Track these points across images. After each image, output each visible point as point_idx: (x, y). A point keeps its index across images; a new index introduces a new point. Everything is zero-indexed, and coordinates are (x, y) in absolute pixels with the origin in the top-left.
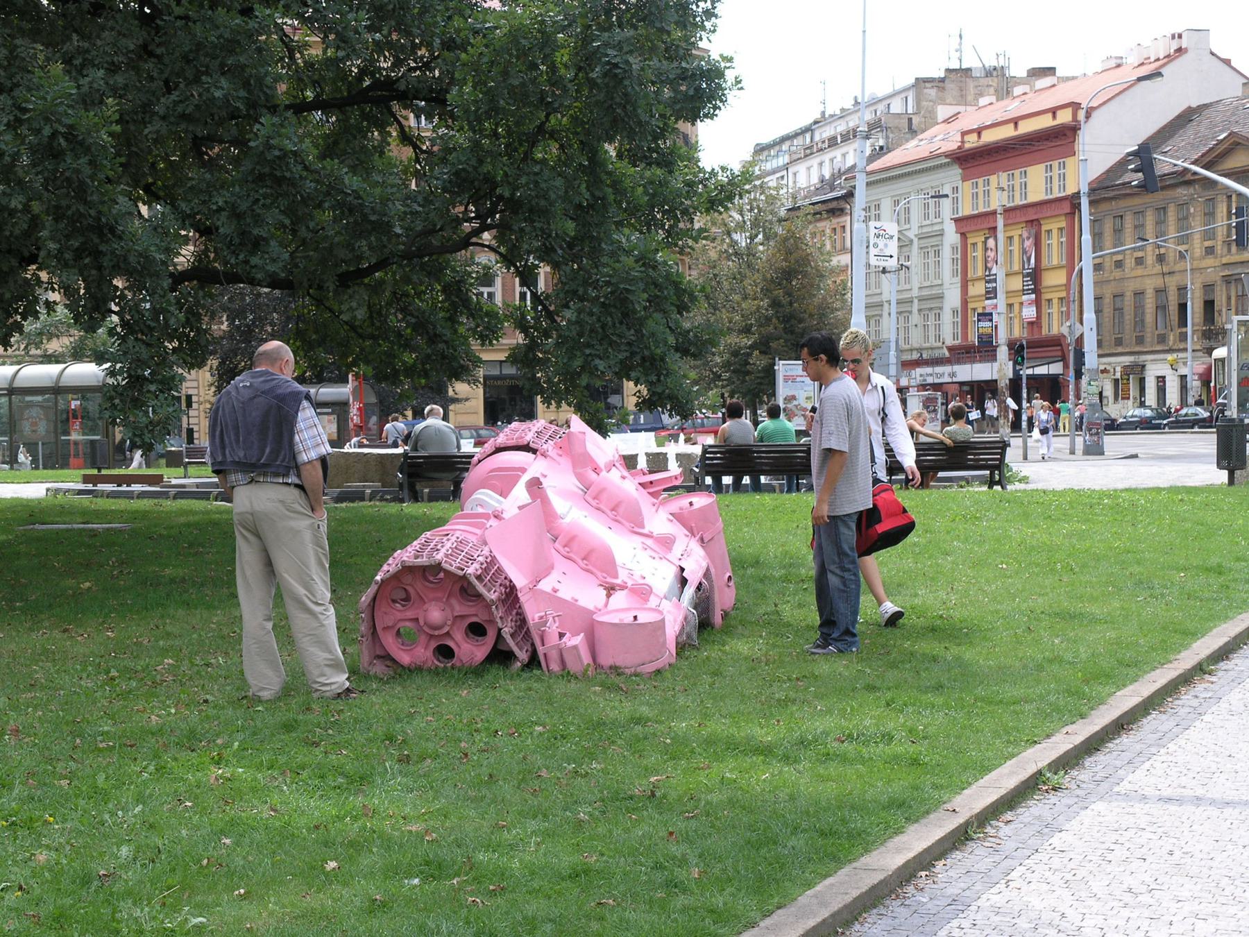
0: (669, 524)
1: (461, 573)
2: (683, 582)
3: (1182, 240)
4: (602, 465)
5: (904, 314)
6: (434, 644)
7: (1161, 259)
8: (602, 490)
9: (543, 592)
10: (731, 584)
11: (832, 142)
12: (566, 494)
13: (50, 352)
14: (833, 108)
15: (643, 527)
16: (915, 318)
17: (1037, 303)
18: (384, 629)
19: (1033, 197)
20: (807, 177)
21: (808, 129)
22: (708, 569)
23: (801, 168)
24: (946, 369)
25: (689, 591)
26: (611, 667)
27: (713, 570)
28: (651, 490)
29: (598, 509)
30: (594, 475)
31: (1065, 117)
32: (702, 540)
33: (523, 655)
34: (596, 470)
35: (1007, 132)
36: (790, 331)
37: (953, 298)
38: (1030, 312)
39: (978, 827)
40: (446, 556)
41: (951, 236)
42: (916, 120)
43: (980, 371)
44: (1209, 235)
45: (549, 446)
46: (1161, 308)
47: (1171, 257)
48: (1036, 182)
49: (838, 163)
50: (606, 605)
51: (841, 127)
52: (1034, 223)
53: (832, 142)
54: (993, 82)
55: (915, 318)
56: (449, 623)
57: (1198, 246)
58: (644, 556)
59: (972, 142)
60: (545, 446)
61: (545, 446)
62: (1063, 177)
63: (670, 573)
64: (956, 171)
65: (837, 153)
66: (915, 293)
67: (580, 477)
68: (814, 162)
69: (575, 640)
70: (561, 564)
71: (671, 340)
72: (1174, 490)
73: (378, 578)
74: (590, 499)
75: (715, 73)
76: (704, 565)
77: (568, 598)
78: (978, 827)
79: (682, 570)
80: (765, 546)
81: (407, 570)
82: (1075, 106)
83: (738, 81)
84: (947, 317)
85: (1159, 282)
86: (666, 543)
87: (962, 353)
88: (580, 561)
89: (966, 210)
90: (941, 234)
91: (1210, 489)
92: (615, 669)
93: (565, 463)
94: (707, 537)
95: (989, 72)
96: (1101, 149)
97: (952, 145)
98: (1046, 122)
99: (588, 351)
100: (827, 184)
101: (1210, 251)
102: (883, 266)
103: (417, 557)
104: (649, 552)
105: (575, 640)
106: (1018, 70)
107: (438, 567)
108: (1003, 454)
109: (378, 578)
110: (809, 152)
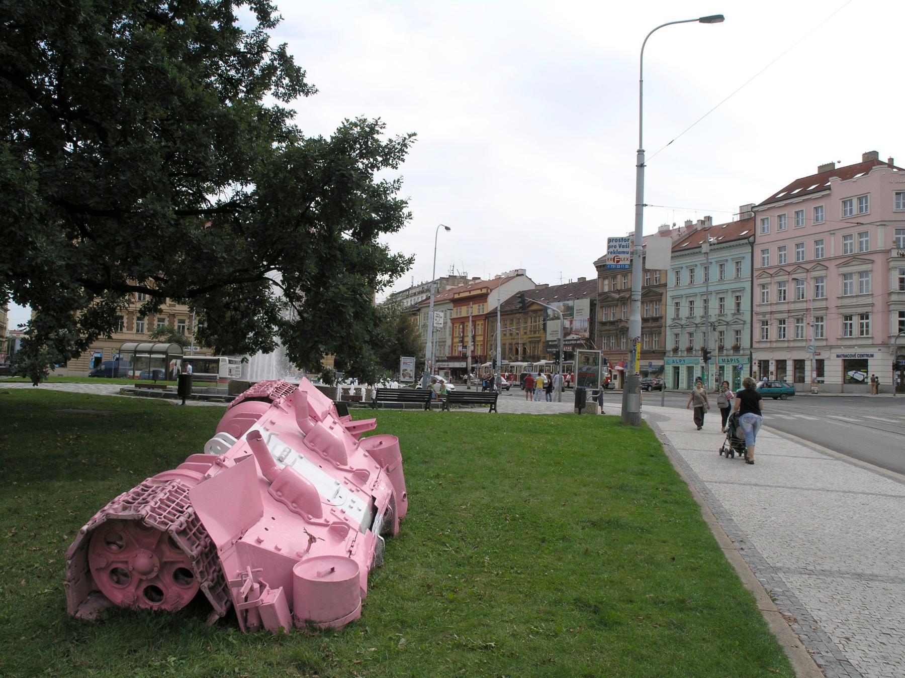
0: (365, 459)
1: (163, 528)
2: (374, 510)
3: (518, 329)
4: (319, 414)
6: (144, 585)
7: (511, 334)
8: (317, 436)
9: (245, 544)
10: (406, 499)
11: (415, 294)
12: (287, 436)
14: (415, 285)
15: (346, 464)
18: (97, 569)
20: (408, 303)
22: (392, 495)
25: (379, 518)
26: (306, 621)
27: (395, 494)
28: (354, 433)
29: (313, 450)
30: (312, 424)
31: (484, 291)
32: (387, 470)
33: (220, 609)
34: (315, 418)
35: (467, 294)
36: (402, 347)
37: (449, 342)
39: (110, 33)
40: (153, 510)
41: (449, 324)
43: (463, 365)
44: (525, 328)
45: (282, 401)
46: (511, 349)
47: (514, 334)
48: (475, 309)
49: (417, 301)
50: (308, 550)
51: (418, 290)
53: (415, 294)
56: (156, 569)
57: (522, 332)
58: (344, 490)
59: (457, 296)
60: (278, 400)
61: (278, 400)
63: (364, 505)
64: (452, 305)
65: (416, 298)
67: (301, 425)
68: (409, 300)
69: (273, 597)
70: (270, 509)
71: (367, 338)
72: (561, 415)
73: (85, 528)
74: (274, 493)
75: (398, 206)
76: (390, 492)
77: (271, 548)
78: (110, 33)
79: (374, 499)
81: (111, 523)
82: (487, 288)
83: (410, 215)
84: (447, 348)
85: (510, 341)
86: (361, 476)
87: (452, 359)
88: (290, 504)
89: (454, 316)
91: (567, 415)
92: (310, 623)
93: (292, 413)
94: (391, 469)
95: (462, 277)
96: (494, 302)
97: (451, 297)
98: (479, 292)
99: (316, 339)
100: (412, 306)
101: (525, 333)
102: (435, 328)
103: (125, 508)
104: (350, 486)
105: (273, 597)
107: (139, 523)
108: (496, 398)
109: (85, 528)
110: (408, 297)
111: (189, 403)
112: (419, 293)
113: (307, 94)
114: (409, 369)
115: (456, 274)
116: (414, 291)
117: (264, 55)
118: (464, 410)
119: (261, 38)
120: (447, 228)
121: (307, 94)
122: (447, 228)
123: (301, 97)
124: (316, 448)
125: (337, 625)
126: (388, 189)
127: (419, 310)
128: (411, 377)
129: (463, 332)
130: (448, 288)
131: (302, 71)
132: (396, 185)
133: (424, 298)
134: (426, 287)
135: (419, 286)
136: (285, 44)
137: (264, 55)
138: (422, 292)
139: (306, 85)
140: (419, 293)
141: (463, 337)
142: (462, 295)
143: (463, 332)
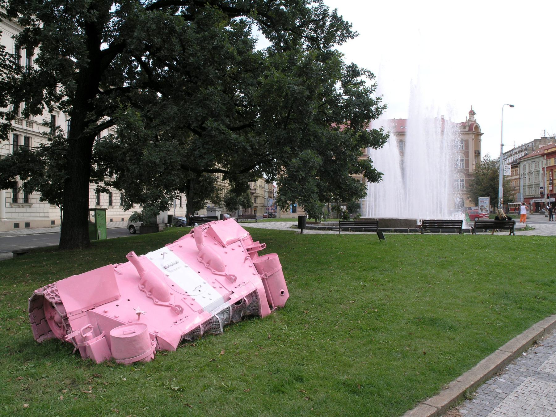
4: (225, 243)
5: (524, 189)
11: (516, 153)
13: (181, 49)
14: (517, 146)
16: (527, 189)
17: (552, 186)
19: (552, 165)
21: (511, 151)
23: (510, 158)
24: (540, 199)
38: (551, 188)
42: (534, 148)
51: (519, 150)
52: (552, 170)
53: (516, 153)
54: (552, 140)
55: (527, 189)
59: (546, 152)
62: (550, 163)
65: (517, 155)
66: (527, 184)
68: (512, 157)
80: (68, 120)
90: (539, 171)
97: (542, 153)
106: (228, 272)
110: (511, 155)
111: (305, 231)
112: (519, 152)
113: (353, 38)
114: (485, 205)
115: (547, 136)
116: (516, 151)
117: (327, 18)
118: (28, 247)
119: (323, 9)
120: (511, 106)
121: (353, 38)
122: (511, 106)
123: (349, 41)
124: (203, 261)
125: (126, 363)
126: (368, 91)
127: (519, 163)
128: (487, 211)
129: (552, 177)
130: (540, 146)
131: (350, 24)
132: (373, 88)
133: (523, 155)
134: (524, 147)
135: (519, 147)
136: (336, 10)
137: (327, 18)
138: (522, 151)
139: (351, 32)
140: (519, 152)
141: (552, 180)
142: (550, 151)
143: (552, 177)
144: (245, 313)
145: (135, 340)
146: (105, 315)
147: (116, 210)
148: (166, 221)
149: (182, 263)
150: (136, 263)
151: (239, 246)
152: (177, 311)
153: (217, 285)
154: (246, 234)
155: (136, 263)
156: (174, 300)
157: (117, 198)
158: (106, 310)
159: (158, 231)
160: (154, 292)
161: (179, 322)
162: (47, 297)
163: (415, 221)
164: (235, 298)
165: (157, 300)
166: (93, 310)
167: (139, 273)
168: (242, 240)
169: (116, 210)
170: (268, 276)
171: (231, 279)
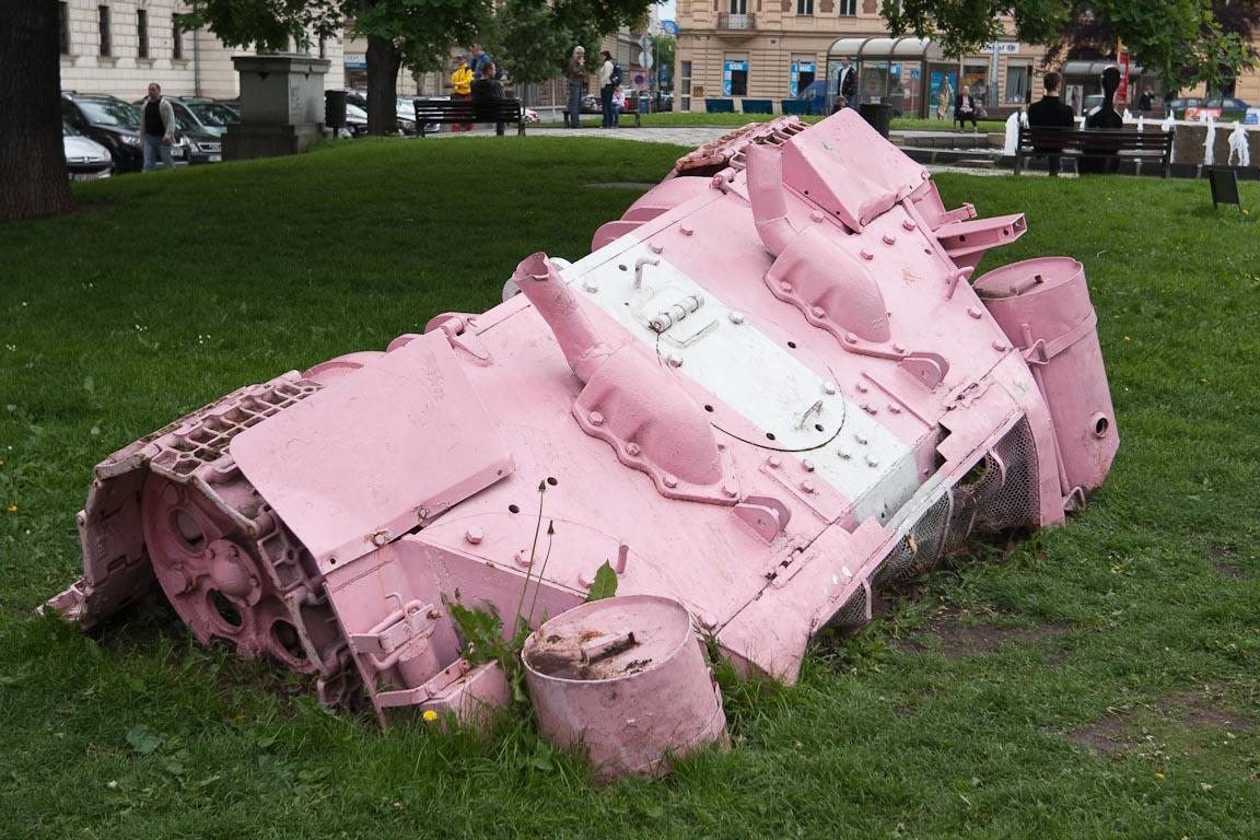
144: (985, 526)
145: (663, 684)
146: (475, 554)
147: (87, 73)
148: (321, 115)
149: (715, 309)
150: (554, 307)
151: (908, 228)
152: (761, 520)
153: (876, 399)
154: (914, 175)
155: (554, 307)
156: (742, 475)
157: (86, 26)
158: (475, 534)
159: (292, 150)
160: (652, 445)
161: (784, 574)
162: (165, 469)
163: (1204, 142)
164: (959, 456)
165: (672, 479)
166: (420, 537)
167: (570, 353)
168: (908, 202)
169: (87, 73)
170: (1049, 355)
171: (927, 370)
